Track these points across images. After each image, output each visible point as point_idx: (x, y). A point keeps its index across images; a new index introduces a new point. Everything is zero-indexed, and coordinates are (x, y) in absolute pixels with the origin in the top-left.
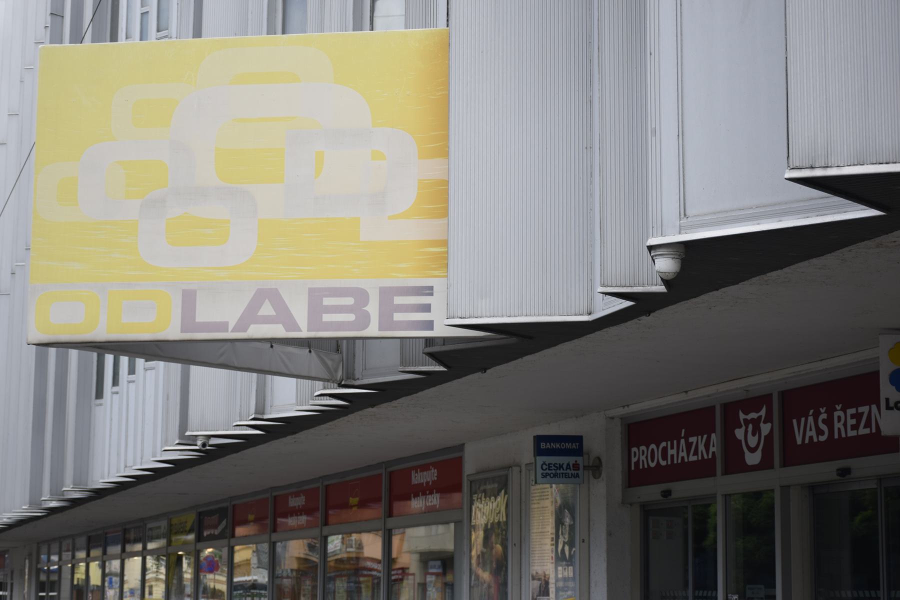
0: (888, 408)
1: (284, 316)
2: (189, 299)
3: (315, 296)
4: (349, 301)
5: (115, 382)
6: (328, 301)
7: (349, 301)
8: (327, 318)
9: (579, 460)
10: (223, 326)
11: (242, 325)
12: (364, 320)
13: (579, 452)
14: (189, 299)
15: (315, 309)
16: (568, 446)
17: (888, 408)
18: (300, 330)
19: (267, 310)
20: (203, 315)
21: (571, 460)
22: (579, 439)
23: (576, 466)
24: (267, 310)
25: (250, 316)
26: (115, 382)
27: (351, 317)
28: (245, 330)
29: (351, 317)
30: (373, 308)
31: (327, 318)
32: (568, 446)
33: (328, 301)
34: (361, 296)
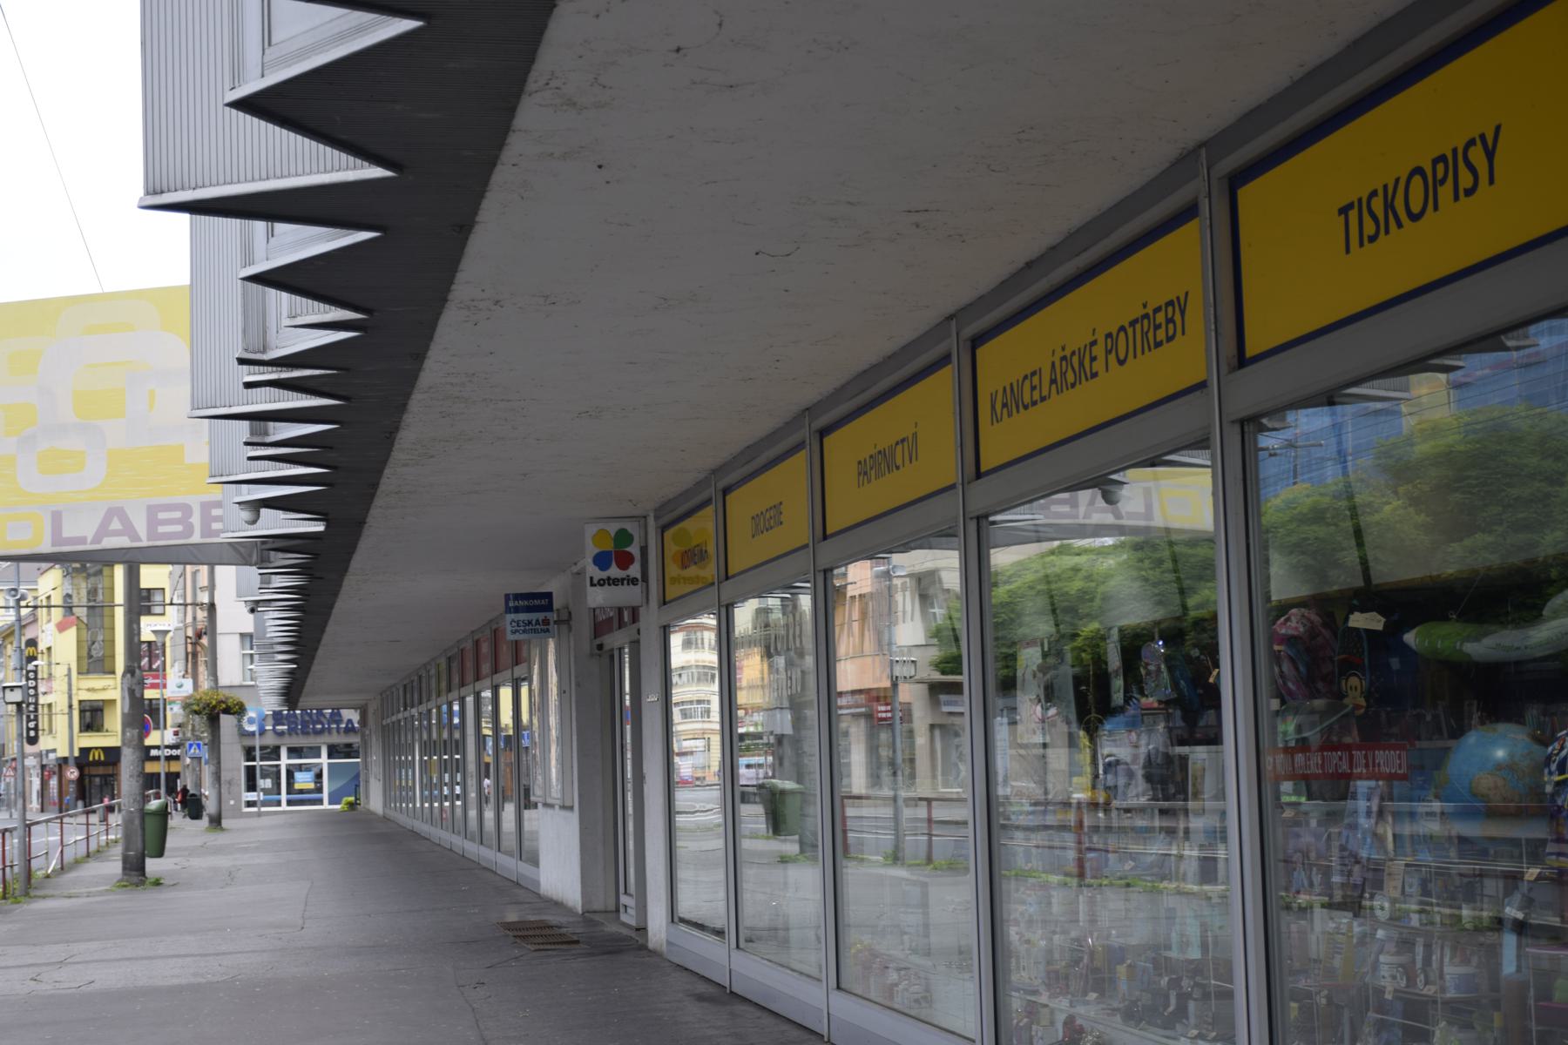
0: (592, 585)
1: (129, 530)
2: (57, 518)
3: (152, 511)
4: (178, 515)
5: (1397, 180)
6: (162, 516)
7: (178, 515)
8: (161, 529)
9: (548, 615)
10: (83, 540)
11: (97, 539)
12: (189, 530)
13: (549, 608)
14: (57, 518)
15: (153, 522)
16: (537, 602)
17: (592, 585)
18: (139, 539)
19: (116, 525)
20: (68, 531)
21: (541, 616)
22: (549, 595)
23: (546, 622)
24: (116, 525)
25: (103, 531)
26: (1397, 180)
27: (179, 528)
28: (99, 542)
29: (179, 528)
30: (196, 520)
31: (161, 529)
32: (537, 602)
33: (162, 516)
34: (186, 509)
